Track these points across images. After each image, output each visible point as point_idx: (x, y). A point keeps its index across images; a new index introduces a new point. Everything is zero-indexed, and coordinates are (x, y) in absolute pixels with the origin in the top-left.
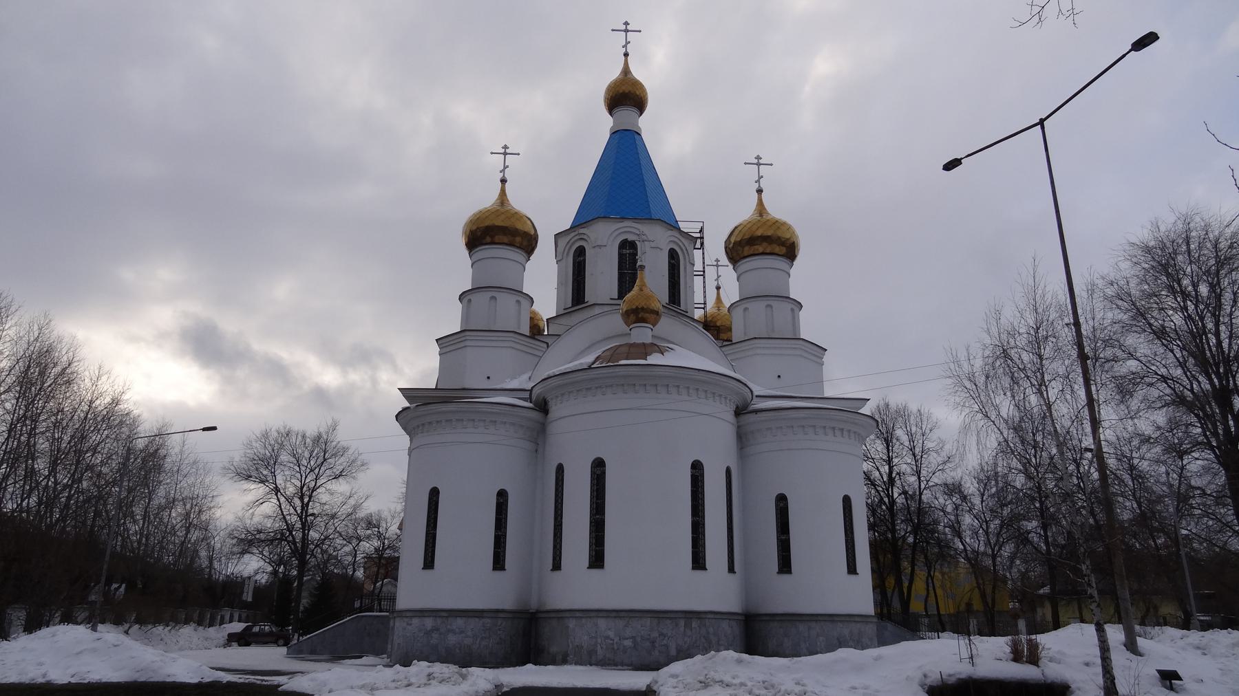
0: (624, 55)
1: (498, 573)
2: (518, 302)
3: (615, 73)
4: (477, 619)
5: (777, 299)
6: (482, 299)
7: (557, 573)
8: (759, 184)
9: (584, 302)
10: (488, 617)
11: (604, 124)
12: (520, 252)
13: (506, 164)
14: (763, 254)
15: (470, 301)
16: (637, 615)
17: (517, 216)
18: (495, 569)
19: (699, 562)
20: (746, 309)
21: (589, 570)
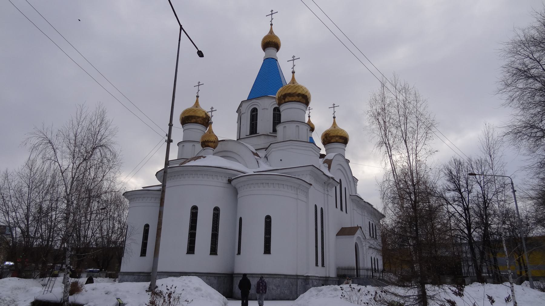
0: (271, 25)
1: (213, 257)
2: (194, 145)
3: (266, 32)
4: (132, 276)
5: (292, 122)
6: (189, 146)
7: (239, 255)
8: (293, 69)
9: (256, 133)
10: (136, 275)
11: (261, 55)
12: (299, 103)
13: (294, 64)
14: (295, 101)
15: (183, 146)
16: (163, 274)
17: (299, 87)
18: (211, 254)
19: (191, 249)
20: (285, 127)
21: (142, 257)
